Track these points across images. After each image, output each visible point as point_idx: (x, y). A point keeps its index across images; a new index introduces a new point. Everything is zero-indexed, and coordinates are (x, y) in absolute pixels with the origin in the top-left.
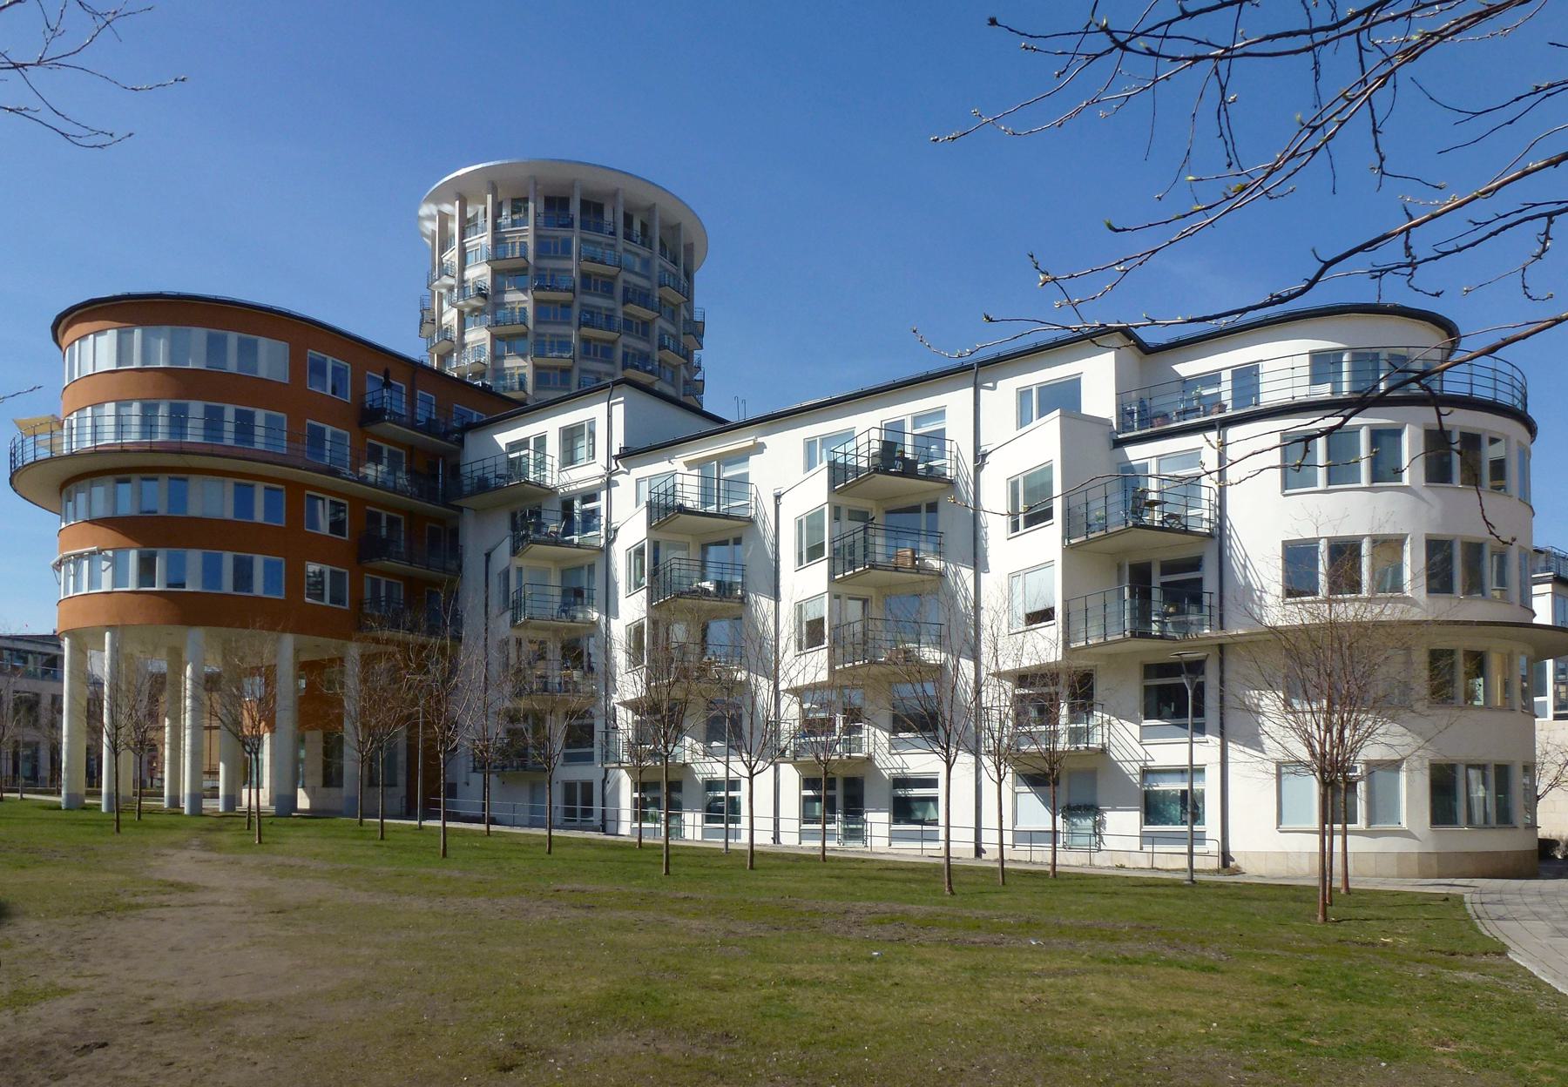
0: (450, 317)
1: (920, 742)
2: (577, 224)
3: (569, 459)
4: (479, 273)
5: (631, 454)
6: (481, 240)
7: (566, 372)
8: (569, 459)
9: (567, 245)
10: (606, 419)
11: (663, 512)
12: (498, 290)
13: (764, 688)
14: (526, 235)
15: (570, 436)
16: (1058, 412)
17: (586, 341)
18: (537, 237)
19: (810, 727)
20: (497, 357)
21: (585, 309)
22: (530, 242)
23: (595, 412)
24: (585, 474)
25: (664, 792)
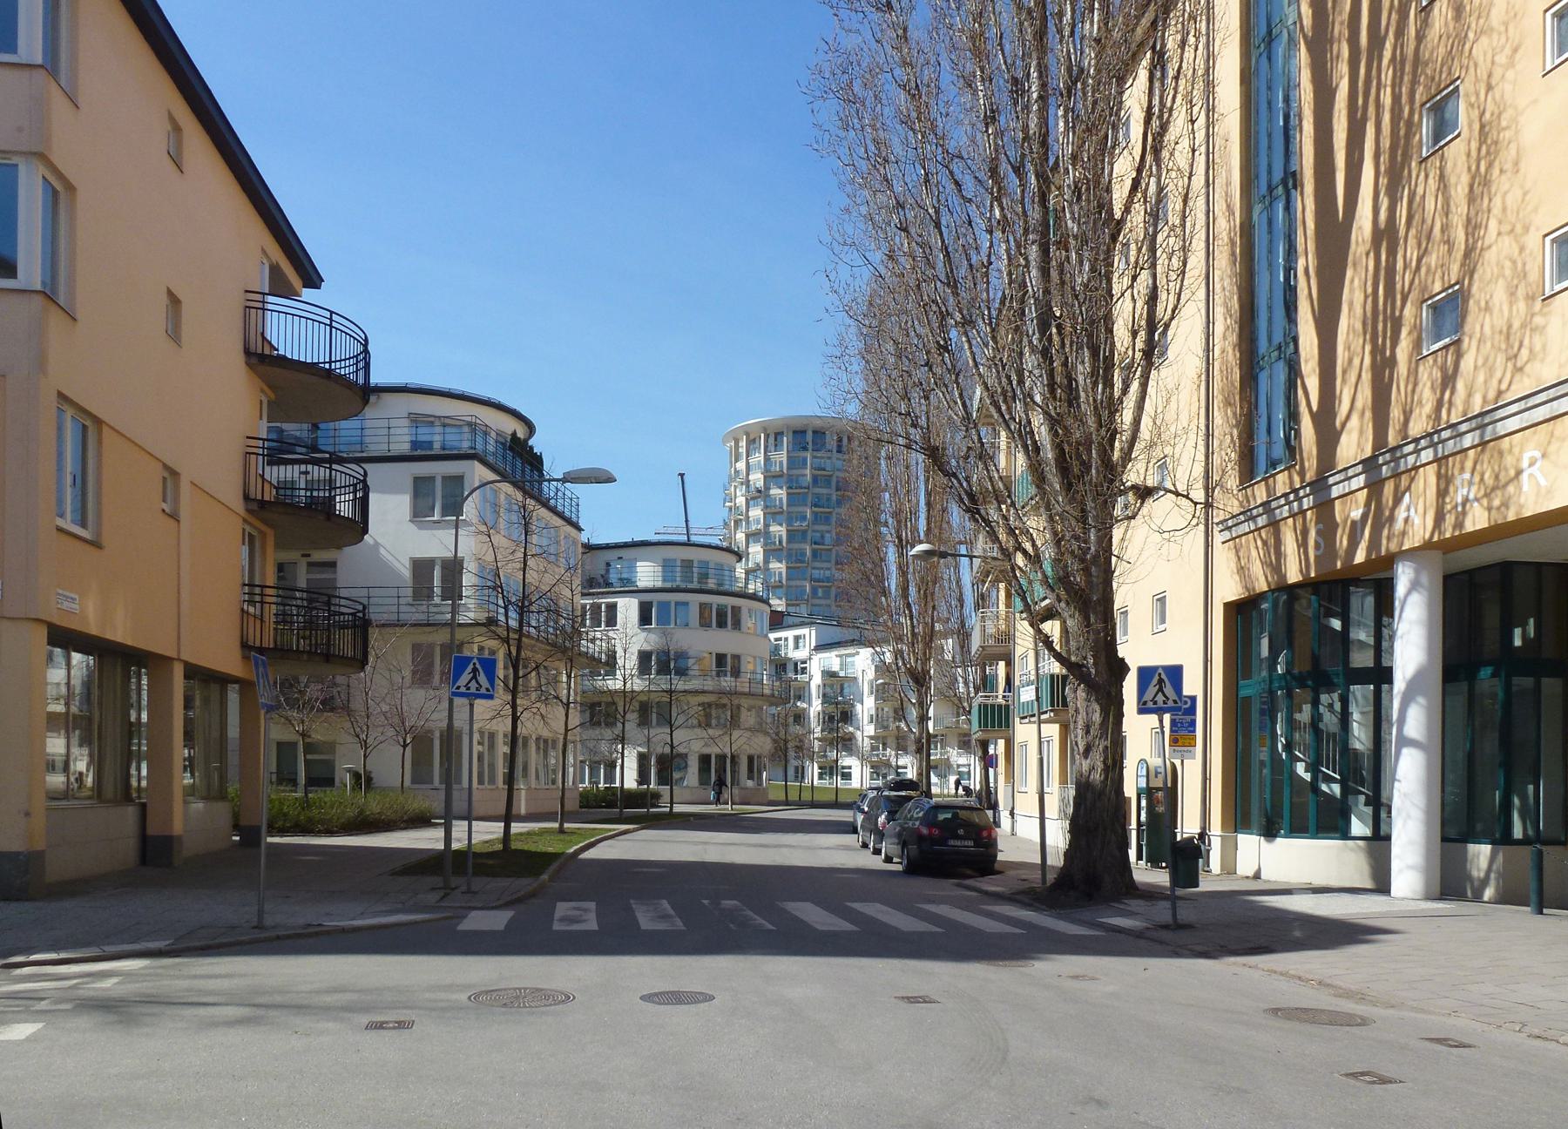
0: (741, 501)
1: (1450, 798)
2: (810, 447)
3: (797, 647)
4: (757, 478)
5: (821, 647)
6: (758, 458)
7: (804, 532)
8: (797, 647)
9: (805, 460)
10: (810, 635)
11: (829, 675)
12: (767, 488)
13: (859, 734)
14: (781, 457)
15: (797, 638)
16: (461, 927)
17: (815, 514)
18: (789, 458)
19: (874, 748)
20: (767, 525)
21: (818, 496)
22: (785, 460)
23: (804, 631)
24: (800, 654)
25: (829, 769)
